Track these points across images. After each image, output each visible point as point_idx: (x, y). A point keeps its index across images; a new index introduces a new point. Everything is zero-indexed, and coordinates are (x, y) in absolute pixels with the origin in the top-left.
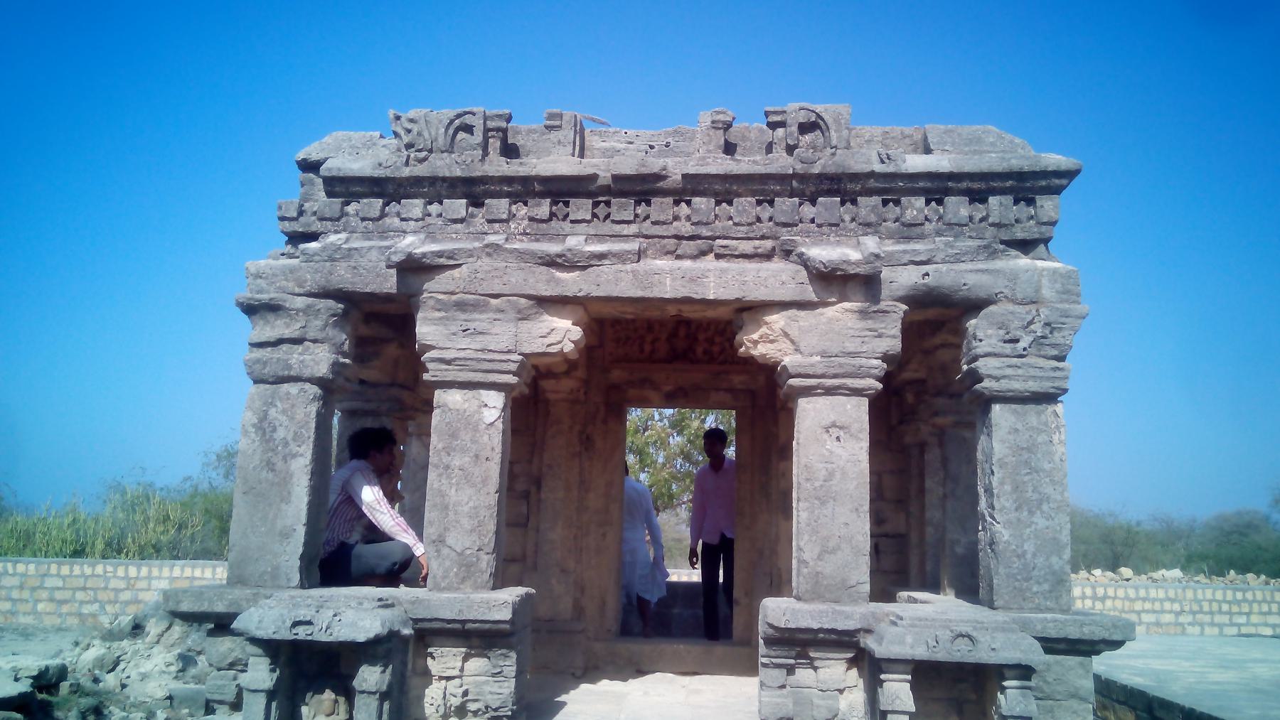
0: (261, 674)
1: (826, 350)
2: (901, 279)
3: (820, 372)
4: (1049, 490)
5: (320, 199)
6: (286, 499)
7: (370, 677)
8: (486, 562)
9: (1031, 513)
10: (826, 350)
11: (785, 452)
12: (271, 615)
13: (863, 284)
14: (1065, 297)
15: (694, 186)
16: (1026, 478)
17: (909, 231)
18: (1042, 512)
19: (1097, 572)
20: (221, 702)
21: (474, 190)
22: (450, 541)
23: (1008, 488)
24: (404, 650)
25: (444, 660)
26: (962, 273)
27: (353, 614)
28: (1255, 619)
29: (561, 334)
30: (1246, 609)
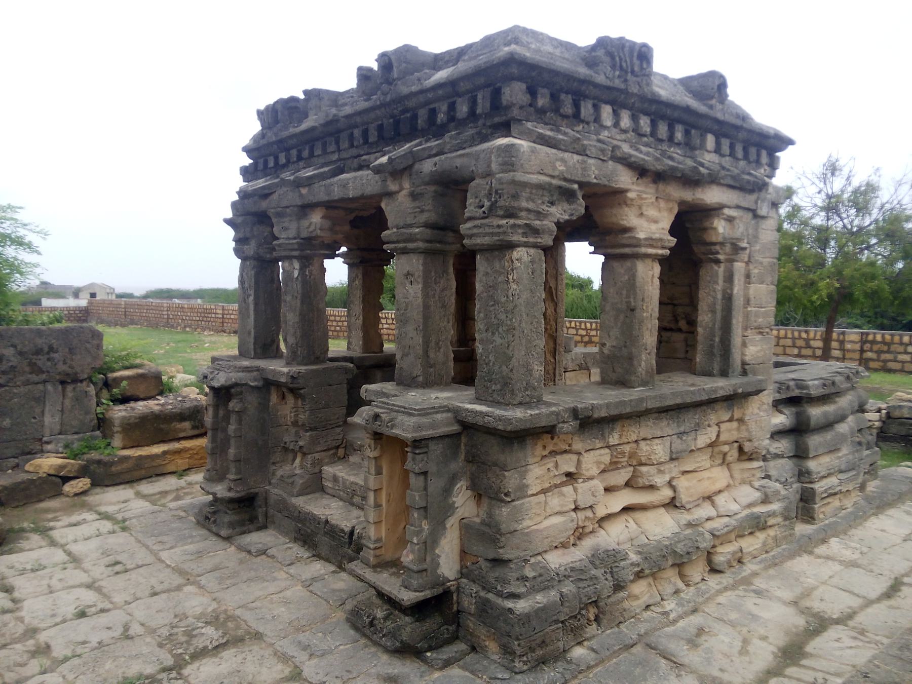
3: (395, 239)
4: (503, 317)
6: (249, 317)
8: (125, 675)
9: (493, 334)
14: (505, 167)
16: (492, 308)
18: (499, 333)
20: (71, 620)
22: (743, 265)
23: (482, 315)
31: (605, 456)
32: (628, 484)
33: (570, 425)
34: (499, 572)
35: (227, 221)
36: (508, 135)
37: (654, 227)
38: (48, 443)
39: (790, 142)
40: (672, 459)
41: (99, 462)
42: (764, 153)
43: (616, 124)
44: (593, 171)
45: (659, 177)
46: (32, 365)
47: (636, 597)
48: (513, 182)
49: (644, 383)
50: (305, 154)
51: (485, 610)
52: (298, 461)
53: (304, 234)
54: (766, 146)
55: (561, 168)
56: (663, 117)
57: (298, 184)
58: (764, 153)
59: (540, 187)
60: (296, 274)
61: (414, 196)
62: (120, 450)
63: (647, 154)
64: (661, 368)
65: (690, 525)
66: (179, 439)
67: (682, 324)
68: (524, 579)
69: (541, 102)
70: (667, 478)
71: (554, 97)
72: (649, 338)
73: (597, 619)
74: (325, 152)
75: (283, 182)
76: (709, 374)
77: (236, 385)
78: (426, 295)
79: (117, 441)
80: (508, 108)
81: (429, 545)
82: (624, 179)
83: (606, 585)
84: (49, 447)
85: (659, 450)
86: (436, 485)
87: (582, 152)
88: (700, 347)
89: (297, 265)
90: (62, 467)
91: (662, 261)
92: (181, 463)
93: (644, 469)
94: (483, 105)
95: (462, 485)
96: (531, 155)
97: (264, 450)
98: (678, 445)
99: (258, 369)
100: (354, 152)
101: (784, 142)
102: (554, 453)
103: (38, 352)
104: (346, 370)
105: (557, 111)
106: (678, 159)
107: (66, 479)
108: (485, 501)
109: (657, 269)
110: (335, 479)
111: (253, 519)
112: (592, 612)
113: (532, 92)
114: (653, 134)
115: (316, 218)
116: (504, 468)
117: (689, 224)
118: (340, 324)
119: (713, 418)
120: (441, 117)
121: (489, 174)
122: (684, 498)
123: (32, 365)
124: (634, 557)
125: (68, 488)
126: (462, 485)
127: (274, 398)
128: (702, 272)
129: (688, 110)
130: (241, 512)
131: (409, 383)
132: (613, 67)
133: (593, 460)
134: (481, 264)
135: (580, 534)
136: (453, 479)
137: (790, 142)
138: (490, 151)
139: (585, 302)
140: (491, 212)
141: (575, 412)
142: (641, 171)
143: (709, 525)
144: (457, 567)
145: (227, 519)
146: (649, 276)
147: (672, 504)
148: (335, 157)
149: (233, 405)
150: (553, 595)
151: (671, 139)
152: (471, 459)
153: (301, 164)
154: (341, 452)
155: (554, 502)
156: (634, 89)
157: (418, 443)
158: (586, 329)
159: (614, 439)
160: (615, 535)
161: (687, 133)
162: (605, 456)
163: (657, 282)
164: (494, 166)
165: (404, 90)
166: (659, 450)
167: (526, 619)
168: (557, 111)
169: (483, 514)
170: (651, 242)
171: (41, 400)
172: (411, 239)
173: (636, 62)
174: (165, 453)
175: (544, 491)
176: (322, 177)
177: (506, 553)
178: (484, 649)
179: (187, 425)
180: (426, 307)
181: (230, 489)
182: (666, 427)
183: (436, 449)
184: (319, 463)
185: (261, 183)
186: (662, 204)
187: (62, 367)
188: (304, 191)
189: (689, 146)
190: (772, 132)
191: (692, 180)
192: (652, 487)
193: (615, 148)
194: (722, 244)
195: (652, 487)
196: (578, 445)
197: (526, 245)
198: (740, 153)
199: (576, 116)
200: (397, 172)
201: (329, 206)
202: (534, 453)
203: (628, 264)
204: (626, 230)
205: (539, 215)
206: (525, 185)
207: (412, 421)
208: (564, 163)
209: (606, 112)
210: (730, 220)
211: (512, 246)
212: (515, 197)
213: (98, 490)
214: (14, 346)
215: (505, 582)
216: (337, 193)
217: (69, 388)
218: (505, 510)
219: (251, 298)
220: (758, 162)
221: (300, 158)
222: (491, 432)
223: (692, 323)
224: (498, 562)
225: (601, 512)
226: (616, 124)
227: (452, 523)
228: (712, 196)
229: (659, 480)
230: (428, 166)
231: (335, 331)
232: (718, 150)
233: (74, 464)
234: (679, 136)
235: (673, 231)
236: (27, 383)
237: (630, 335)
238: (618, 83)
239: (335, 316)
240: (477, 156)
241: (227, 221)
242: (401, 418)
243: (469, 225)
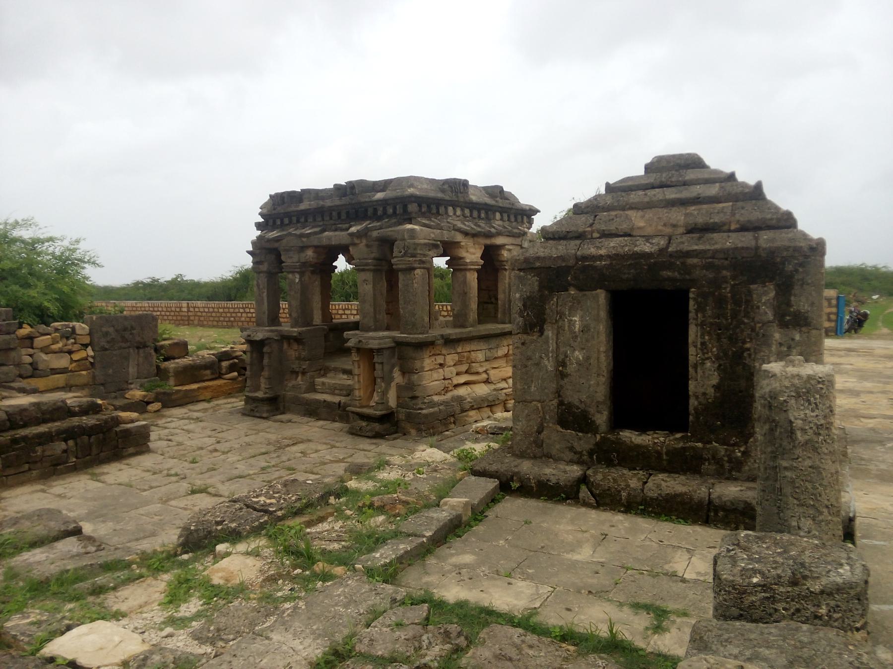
31: (456, 357)
32: (466, 372)
33: (440, 342)
34: (414, 402)
35: (248, 252)
36: (411, 223)
37: (473, 257)
38: (131, 384)
39: (539, 211)
40: (486, 361)
41: (164, 393)
42: (525, 217)
43: (455, 214)
44: (446, 236)
45: (474, 235)
46: (123, 337)
47: (471, 417)
48: (415, 244)
49: (472, 326)
50: (302, 220)
51: (409, 417)
52: (299, 378)
53: (303, 260)
54: (528, 213)
55: (433, 236)
56: (475, 208)
57: (302, 236)
58: (525, 217)
59: (425, 244)
60: (297, 280)
61: (367, 246)
62: (171, 386)
63: (468, 226)
64: (480, 321)
65: (495, 390)
66: (204, 381)
67: (493, 300)
68: (425, 403)
69: (423, 210)
70: (484, 369)
71: (429, 207)
72: (474, 305)
73: (454, 423)
74: (315, 220)
75: (290, 234)
76: (504, 323)
77: (268, 339)
78: (374, 289)
79: (172, 382)
80: (411, 213)
81: (384, 393)
82: (459, 237)
83: (457, 409)
84: (132, 386)
85: (480, 356)
86: (387, 368)
87: (441, 229)
88: (500, 310)
89: (297, 276)
90: (145, 396)
91: (478, 271)
92: (208, 395)
93: (474, 364)
94: (399, 210)
95: (396, 369)
96: (418, 230)
97: (281, 373)
98: (489, 354)
99: (276, 331)
100: (332, 222)
101: (536, 211)
102: (434, 355)
103: (125, 329)
104: (324, 329)
105: (430, 212)
106: (483, 226)
107: (148, 403)
108: (407, 375)
109: (476, 275)
110: (323, 384)
111: (277, 409)
112: (452, 420)
113: (420, 206)
114: (471, 216)
115: (310, 253)
116: (415, 359)
117: (491, 254)
118: (234, 315)
119: (505, 342)
120: (380, 213)
121: (404, 240)
122: (492, 378)
123: (123, 337)
124: (469, 400)
125: (150, 407)
126: (396, 369)
127: (285, 346)
128: (499, 274)
129: (486, 204)
130: (272, 406)
131: (368, 330)
132: (452, 192)
133: (451, 359)
134: (401, 276)
135: (446, 390)
136: (393, 367)
137: (539, 211)
138: (404, 230)
139: (446, 289)
140: (405, 255)
141: (442, 336)
142: (466, 234)
143: (504, 391)
144: (396, 403)
145: (265, 409)
146: (472, 278)
147: (487, 381)
148: (321, 223)
149: (266, 349)
150: (436, 409)
151: (479, 217)
152: (400, 358)
153: (299, 225)
154: (322, 372)
155: (435, 375)
156: (462, 200)
157: (379, 350)
158: (447, 311)
159: (459, 350)
160: (462, 391)
161: (487, 213)
162: (456, 357)
163: (476, 280)
164: (406, 237)
165: (362, 200)
166: (480, 356)
167: (426, 416)
168: (430, 212)
169: (406, 381)
170: (472, 263)
171: (127, 358)
172: (367, 264)
173: (462, 187)
174: (199, 388)
175: (431, 370)
176: (315, 233)
177: (417, 394)
178: (409, 433)
179: (208, 372)
180: (375, 295)
181: (265, 393)
182: (483, 345)
183: (386, 353)
184: (313, 377)
185: (274, 234)
186: (477, 246)
187: (138, 339)
188: (304, 240)
189: (488, 219)
190: (528, 208)
191: (489, 235)
192: (478, 373)
193: (454, 225)
194: (507, 261)
195: (478, 373)
196: (444, 352)
197: (420, 268)
198: (513, 219)
199: (438, 213)
200: (359, 235)
201: (316, 247)
202: (426, 353)
203: (463, 273)
204: (462, 258)
205: (425, 255)
206: (418, 244)
207: (377, 342)
208: (434, 234)
209: (450, 209)
210: (509, 250)
211: (414, 269)
212: (415, 249)
213: (165, 410)
214: (113, 326)
215: (417, 404)
216: (325, 242)
217: (141, 351)
218: (416, 376)
219: (265, 294)
220: (522, 222)
221: (298, 221)
222: (408, 344)
223: (497, 299)
224: (414, 398)
225: (455, 382)
226: (455, 214)
227: (393, 384)
228: (499, 241)
229: (481, 370)
230: (375, 234)
231: (229, 321)
232: (502, 219)
233: (151, 395)
234: (483, 215)
235: (482, 258)
236: (120, 348)
237: (465, 305)
238: (454, 198)
239: (229, 308)
240: (398, 231)
241: (248, 252)
242: (371, 341)
243: (395, 260)
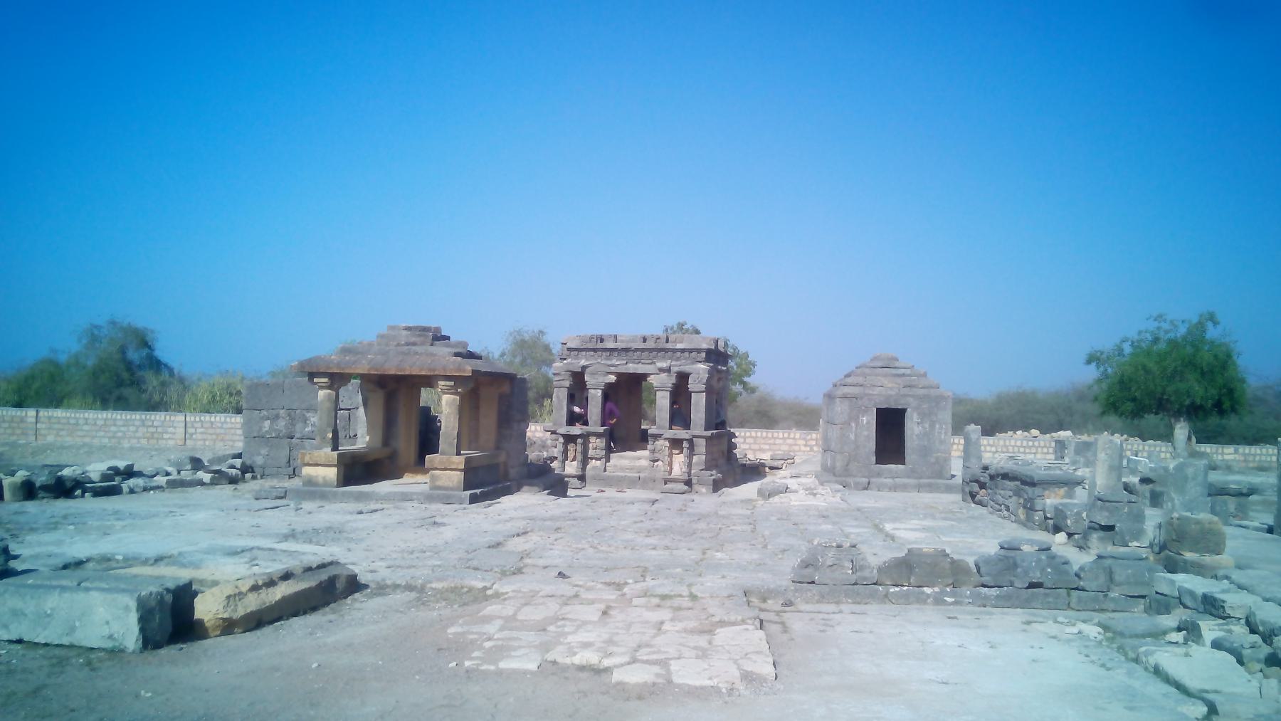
0: (561, 440)
1: (660, 383)
2: (675, 369)
5: (566, 352)
7: (579, 441)
10: (660, 383)
11: (420, 432)
12: (564, 430)
13: (668, 370)
15: (637, 350)
17: (678, 359)
19: (1019, 432)
21: (595, 350)
24: (586, 437)
25: (592, 439)
26: (686, 368)
27: (577, 430)
28: (1039, 456)
29: (612, 378)
30: (1034, 450)
